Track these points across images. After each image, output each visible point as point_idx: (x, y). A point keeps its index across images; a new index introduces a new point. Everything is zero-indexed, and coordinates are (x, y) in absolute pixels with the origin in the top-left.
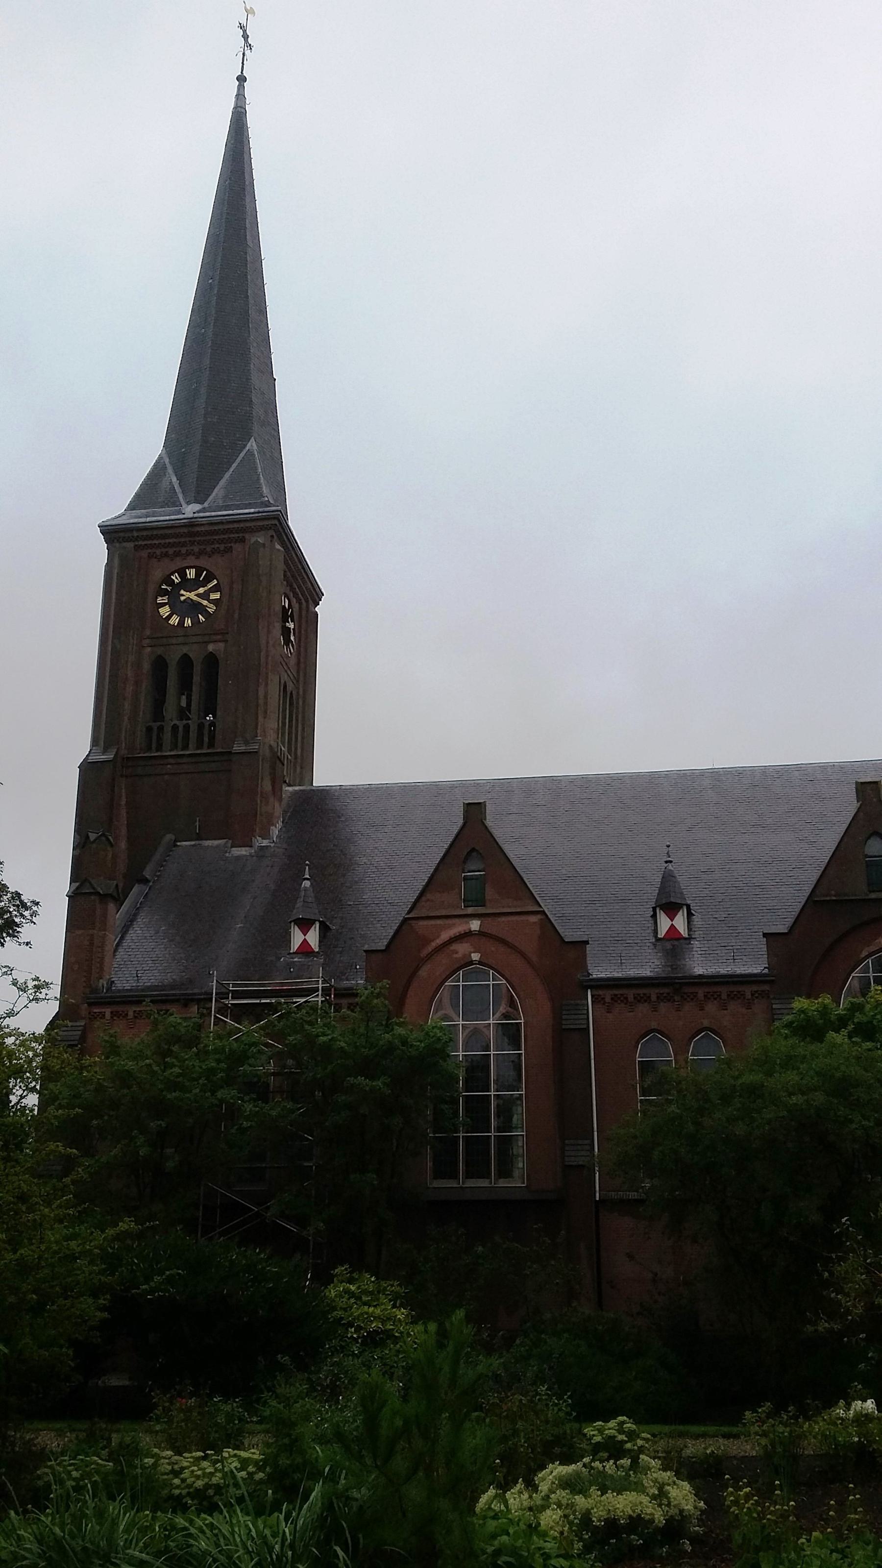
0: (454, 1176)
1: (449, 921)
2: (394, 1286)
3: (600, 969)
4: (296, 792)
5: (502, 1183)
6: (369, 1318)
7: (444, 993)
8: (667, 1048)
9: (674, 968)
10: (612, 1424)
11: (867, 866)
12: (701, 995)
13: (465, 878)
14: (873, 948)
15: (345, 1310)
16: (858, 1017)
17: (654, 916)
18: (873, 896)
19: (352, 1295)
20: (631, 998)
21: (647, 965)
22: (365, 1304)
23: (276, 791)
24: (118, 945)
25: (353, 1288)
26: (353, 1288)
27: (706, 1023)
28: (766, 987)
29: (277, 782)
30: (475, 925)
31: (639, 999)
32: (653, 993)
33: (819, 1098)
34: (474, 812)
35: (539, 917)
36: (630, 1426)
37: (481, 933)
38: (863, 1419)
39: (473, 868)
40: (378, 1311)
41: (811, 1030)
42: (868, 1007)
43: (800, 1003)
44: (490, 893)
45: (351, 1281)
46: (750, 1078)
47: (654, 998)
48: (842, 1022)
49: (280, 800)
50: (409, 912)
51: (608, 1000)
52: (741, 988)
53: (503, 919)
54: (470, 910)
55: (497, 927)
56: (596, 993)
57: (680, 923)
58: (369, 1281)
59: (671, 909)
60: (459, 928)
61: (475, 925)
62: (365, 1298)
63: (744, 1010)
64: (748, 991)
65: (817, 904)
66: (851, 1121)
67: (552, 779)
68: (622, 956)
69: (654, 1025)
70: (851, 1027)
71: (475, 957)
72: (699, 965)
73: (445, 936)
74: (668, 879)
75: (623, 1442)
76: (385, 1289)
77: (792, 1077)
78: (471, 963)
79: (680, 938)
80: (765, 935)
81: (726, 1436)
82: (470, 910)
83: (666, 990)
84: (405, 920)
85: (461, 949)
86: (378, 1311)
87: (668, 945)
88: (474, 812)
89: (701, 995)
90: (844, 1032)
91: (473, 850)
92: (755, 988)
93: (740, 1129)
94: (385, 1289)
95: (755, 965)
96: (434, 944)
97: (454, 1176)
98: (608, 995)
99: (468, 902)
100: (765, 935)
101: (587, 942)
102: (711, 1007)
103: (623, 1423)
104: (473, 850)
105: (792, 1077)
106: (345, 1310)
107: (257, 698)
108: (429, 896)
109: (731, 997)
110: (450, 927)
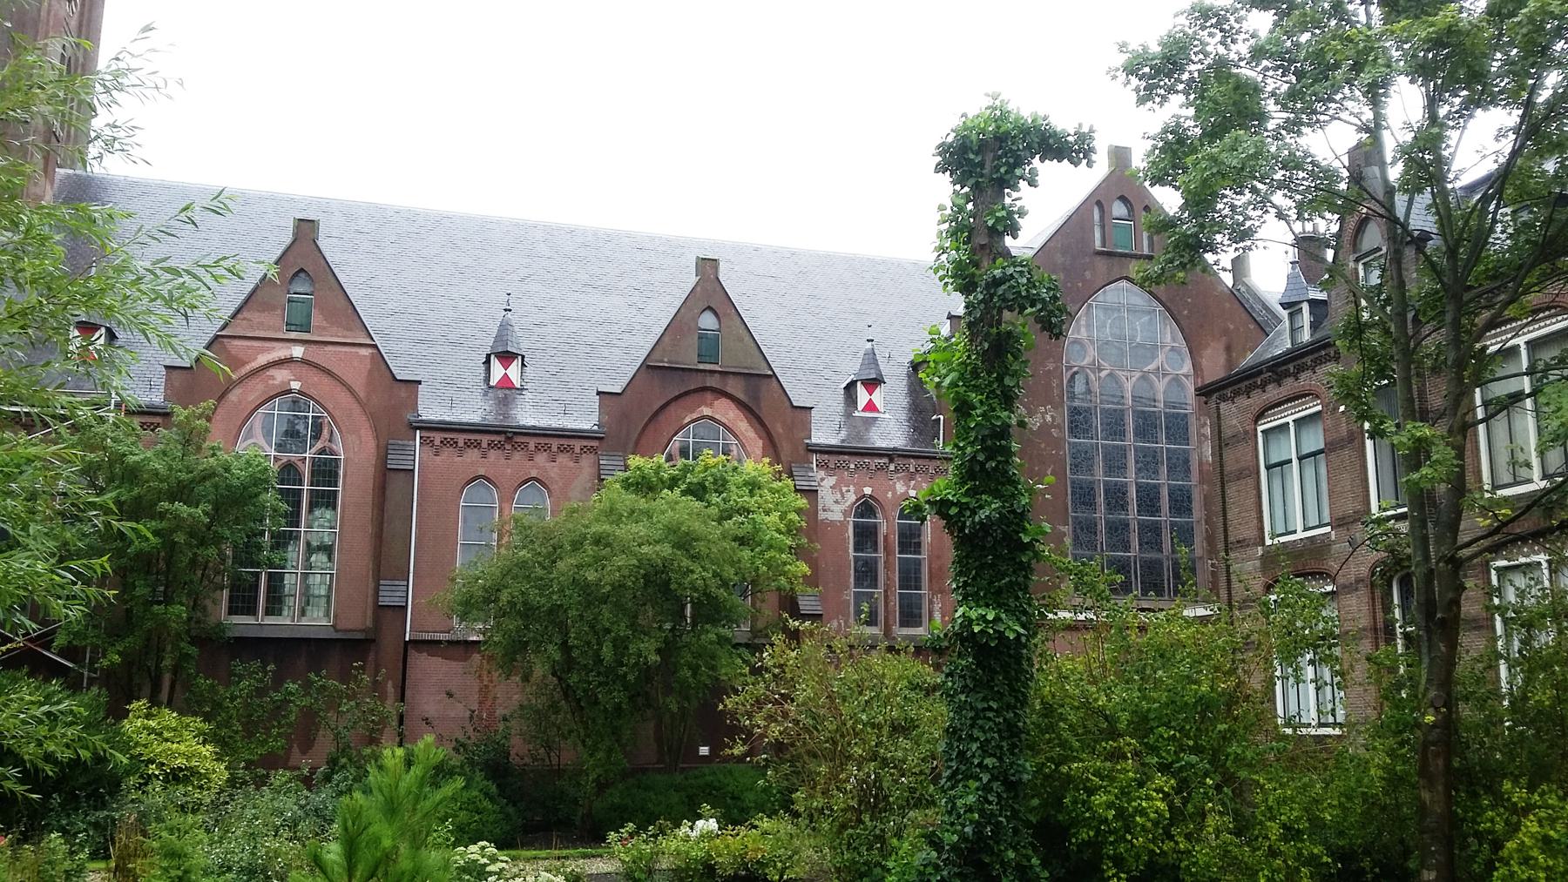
0: (252, 611)
1: (267, 344)
2: (197, 723)
3: (430, 410)
4: (69, 176)
5: (270, 620)
6: (174, 755)
7: (257, 421)
8: (492, 494)
9: (506, 416)
10: (473, 848)
11: (700, 338)
12: (532, 446)
13: (290, 301)
14: (695, 416)
15: (145, 746)
16: (690, 478)
17: (488, 362)
18: (701, 367)
19: (151, 731)
20: (461, 444)
21: (473, 410)
22: (167, 740)
23: (48, 170)
24: (1225, 524)
25: (152, 723)
26: (152, 723)
27: (534, 474)
28: (595, 444)
29: (48, 164)
30: (298, 351)
31: (468, 444)
32: (485, 439)
33: (666, 550)
34: (306, 230)
35: (370, 351)
36: (492, 850)
37: (304, 361)
38: (708, 836)
39: (301, 290)
40: (182, 748)
41: (644, 486)
42: (697, 469)
43: (635, 461)
44: (317, 319)
45: (148, 716)
46: (596, 528)
47: (484, 445)
48: (673, 483)
49: (52, 183)
50: (223, 328)
51: (437, 442)
52: (572, 442)
53: (330, 348)
54: (293, 335)
55: (323, 356)
56: (426, 434)
57: (514, 371)
58: (170, 717)
59: (507, 357)
60: (280, 352)
61: (298, 351)
62: (166, 734)
63: (572, 464)
64: (577, 445)
65: (649, 367)
66: (692, 572)
67: (379, 208)
68: (451, 398)
69: (482, 472)
70: (683, 487)
71: (295, 385)
72: (527, 415)
73: (262, 359)
74: (505, 327)
75: (485, 865)
76: (188, 725)
77: (641, 529)
78: (290, 391)
79: (511, 387)
80: (599, 393)
81: (585, 856)
82: (293, 335)
83: (496, 438)
84: (217, 337)
85: (280, 376)
86: (182, 748)
87: (500, 394)
88: (306, 230)
89: (532, 446)
90: (677, 491)
91: (302, 270)
92: (585, 443)
93: (591, 576)
94: (188, 725)
95: (586, 419)
96: (248, 368)
97: (252, 611)
98: (438, 437)
99: (290, 326)
100: (599, 393)
101: (419, 382)
102: (541, 458)
103: (483, 848)
104: (302, 270)
105: (641, 529)
106: (145, 746)
107: (1480, 480)
108: (245, 314)
109: (561, 449)
110: (268, 350)
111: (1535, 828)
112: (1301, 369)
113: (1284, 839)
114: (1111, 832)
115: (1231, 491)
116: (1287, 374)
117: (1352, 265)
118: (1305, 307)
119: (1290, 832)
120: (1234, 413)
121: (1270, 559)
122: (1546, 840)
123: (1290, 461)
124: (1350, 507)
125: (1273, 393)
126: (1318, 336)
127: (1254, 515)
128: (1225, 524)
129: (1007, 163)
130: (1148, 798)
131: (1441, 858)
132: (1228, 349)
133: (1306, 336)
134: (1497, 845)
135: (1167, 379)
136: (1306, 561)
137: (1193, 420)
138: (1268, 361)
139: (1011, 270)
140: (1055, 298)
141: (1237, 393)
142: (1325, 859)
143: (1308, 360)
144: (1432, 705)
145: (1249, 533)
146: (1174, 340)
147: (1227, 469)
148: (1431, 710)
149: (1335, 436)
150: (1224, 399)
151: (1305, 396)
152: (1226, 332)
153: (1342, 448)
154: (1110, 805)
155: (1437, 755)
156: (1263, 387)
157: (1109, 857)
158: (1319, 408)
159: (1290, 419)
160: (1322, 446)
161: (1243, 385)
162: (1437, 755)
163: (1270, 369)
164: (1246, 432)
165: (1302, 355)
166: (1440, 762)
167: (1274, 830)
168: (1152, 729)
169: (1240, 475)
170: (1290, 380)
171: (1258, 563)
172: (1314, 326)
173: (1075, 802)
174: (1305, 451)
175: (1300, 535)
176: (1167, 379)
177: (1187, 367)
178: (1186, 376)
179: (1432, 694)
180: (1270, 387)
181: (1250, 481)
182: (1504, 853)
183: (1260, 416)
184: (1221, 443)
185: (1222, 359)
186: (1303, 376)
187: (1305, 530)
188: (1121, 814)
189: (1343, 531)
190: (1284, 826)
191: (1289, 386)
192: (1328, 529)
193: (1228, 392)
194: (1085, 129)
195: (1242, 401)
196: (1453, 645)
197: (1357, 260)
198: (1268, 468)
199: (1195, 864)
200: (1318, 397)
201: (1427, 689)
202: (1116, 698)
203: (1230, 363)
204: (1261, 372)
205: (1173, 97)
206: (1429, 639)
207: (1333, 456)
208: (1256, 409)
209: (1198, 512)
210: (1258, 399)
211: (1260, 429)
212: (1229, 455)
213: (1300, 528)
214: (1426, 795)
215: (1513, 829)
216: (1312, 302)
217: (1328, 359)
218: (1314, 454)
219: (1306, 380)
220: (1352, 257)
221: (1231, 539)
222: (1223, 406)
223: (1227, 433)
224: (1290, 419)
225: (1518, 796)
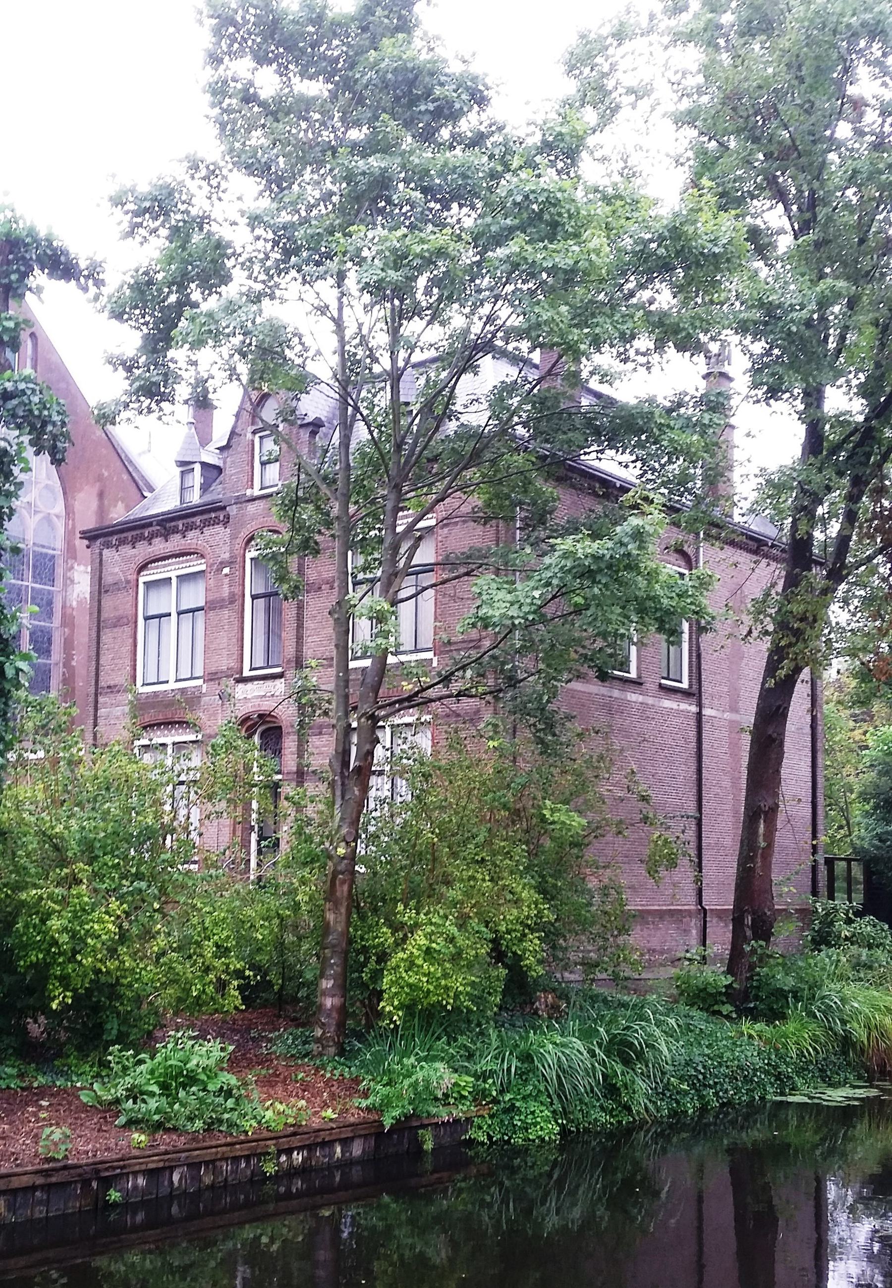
24: (97, 669)
111: (423, 942)
112: (190, 527)
113: (215, 956)
114: (60, 954)
115: (107, 637)
116: (175, 531)
117: (249, 436)
118: (197, 467)
119: (222, 951)
120: (119, 561)
121: (141, 706)
122: (428, 951)
123: (169, 615)
124: (225, 663)
125: (159, 546)
126: (208, 498)
127: (128, 662)
128: (97, 669)
129: (18, 271)
130: (100, 921)
131: (339, 969)
132: (101, 495)
133: (195, 498)
134: (383, 957)
135: (39, 516)
136: (164, 714)
137: (60, 562)
138: (157, 515)
139: (22, 386)
140: (64, 424)
141: (122, 542)
142: (247, 973)
143: (197, 520)
144: (344, 840)
145: (120, 678)
146: (48, 477)
147: (104, 615)
148: (343, 844)
149: (217, 595)
150: (108, 545)
151: (190, 554)
152: (100, 478)
153: (221, 607)
154: (65, 929)
155: (343, 882)
156: (150, 540)
157: (56, 978)
158: (203, 567)
159: (173, 575)
160: (202, 603)
161: (129, 535)
162: (343, 882)
163: (159, 523)
164: (128, 582)
165: (194, 515)
166: (346, 888)
167: (209, 948)
168: (97, 857)
169: (118, 623)
170: (178, 537)
171: (127, 709)
172: (205, 488)
173: (26, 926)
174: (184, 607)
175: (172, 685)
176: (39, 516)
177: (59, 507)
178: (58, 517)
179: (344, 831)
180: (156, 541)
181: (128, 630)
182: (393, 962)
183: (143, 567)
184: (100, 588)
185: (94, 504)
186: (191, 534)
187: (177, 681)
188: (74, 935)
189: (214, 685)
190: (217, 946)
191: (176, 543)
192: (200, 682)
193: (114, 540)
194: (98, 258)
195: (127, 551)
196: (365, 788)
197: (254, 433)
198: (146, 619)
199: (137, 980)
200: (202, 556)
201: (340, 826)
202: (71, 827)
203: (102, 511)
204: (150, 525)
205: (152, 239)
206: (343, 784)
207: (211, 613)
208: (140, 560)
209: (57, 654)
210: (143, 551)
211: (142, 580)
212: (108, 602)
213: (172, 678)
214: (330, 917)
215: (400, 943)
216: (204, 465)
217: (216, 522)
218: (193, 611)
219: (193, 539)
220: (250, 429)
221: (102, 684)
222: (106, 552)
223: (108, 579)
224: (173, 575)
225: (407, 916)
